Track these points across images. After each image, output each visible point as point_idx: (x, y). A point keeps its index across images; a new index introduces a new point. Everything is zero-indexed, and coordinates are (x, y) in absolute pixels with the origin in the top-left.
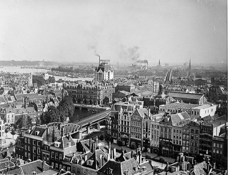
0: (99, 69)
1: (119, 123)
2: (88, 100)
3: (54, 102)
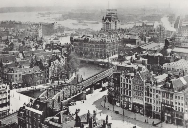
0: (106, 18)
1: (121, 86)
2: (94, 54)
3: (59, 60)
